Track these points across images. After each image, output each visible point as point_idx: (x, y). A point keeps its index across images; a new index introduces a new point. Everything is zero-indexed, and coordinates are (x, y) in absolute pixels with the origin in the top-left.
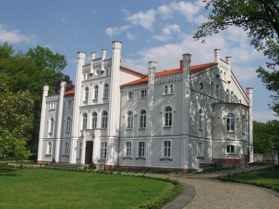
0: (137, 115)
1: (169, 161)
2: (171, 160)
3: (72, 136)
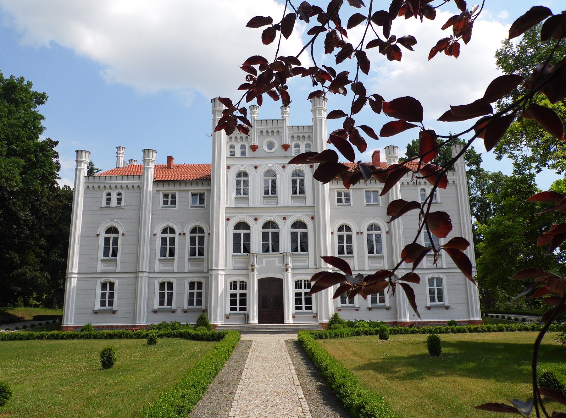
2: (447, 308)
3: (214, 268)
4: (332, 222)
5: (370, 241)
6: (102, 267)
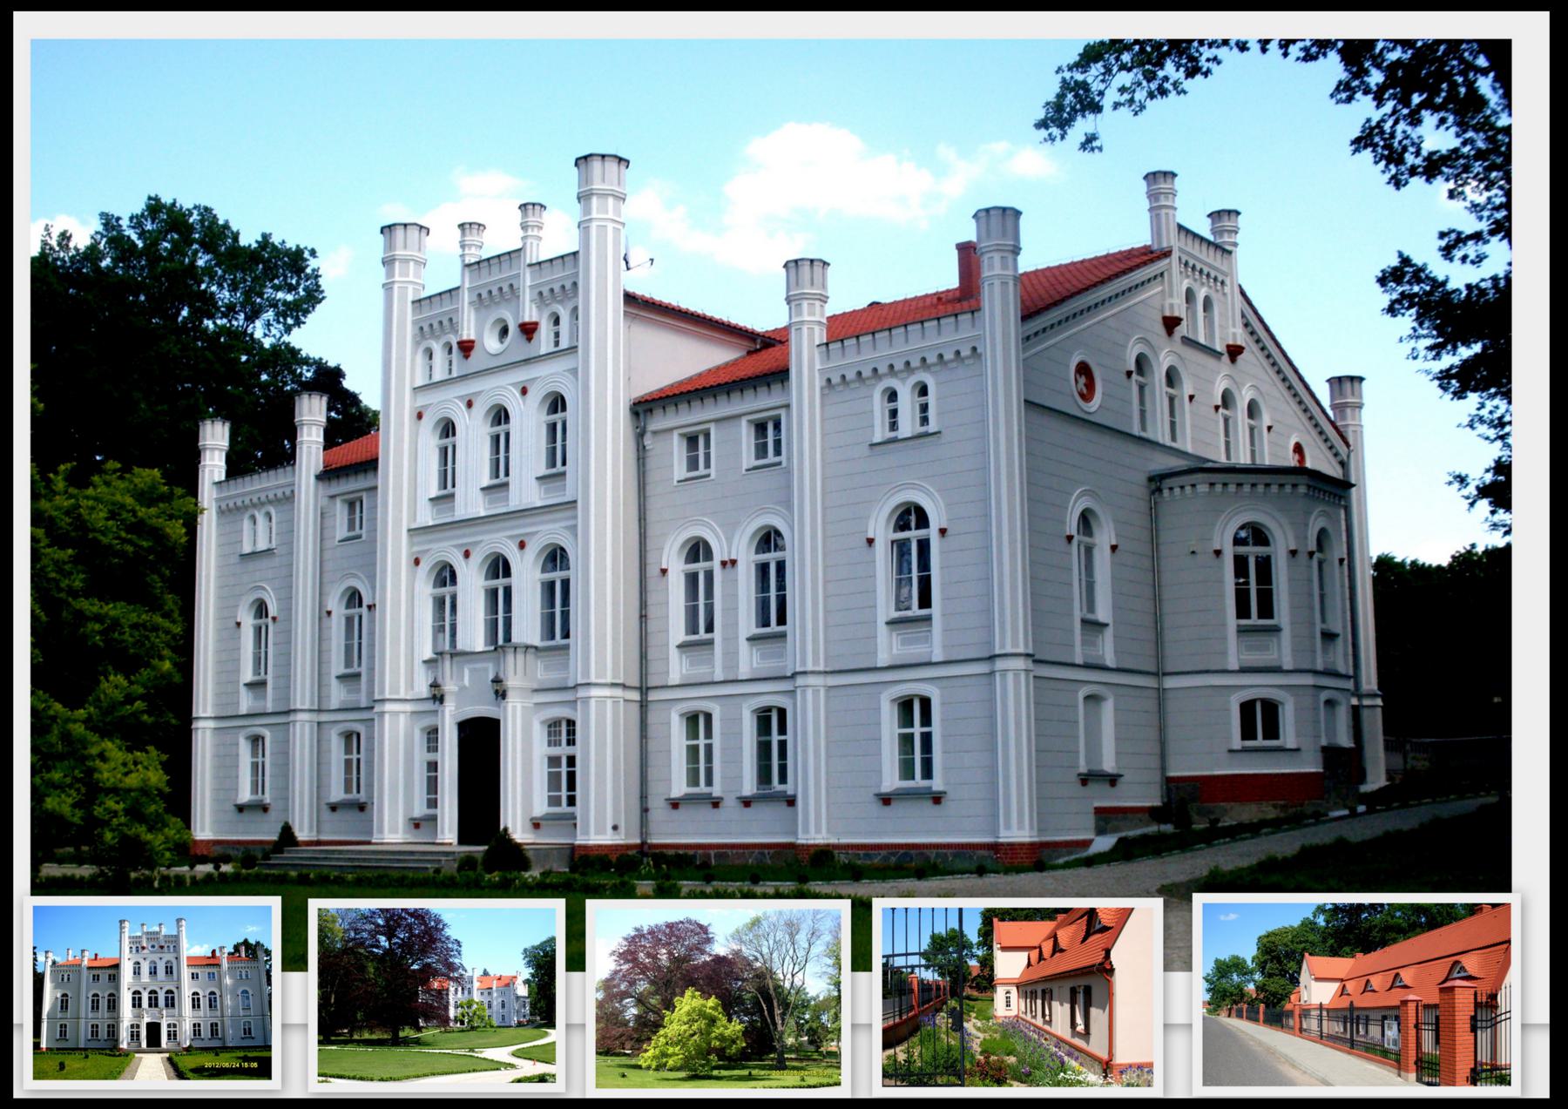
0: (734, 562)
2: (937, 799)
4: (189, 989)
5: (210, 1000)
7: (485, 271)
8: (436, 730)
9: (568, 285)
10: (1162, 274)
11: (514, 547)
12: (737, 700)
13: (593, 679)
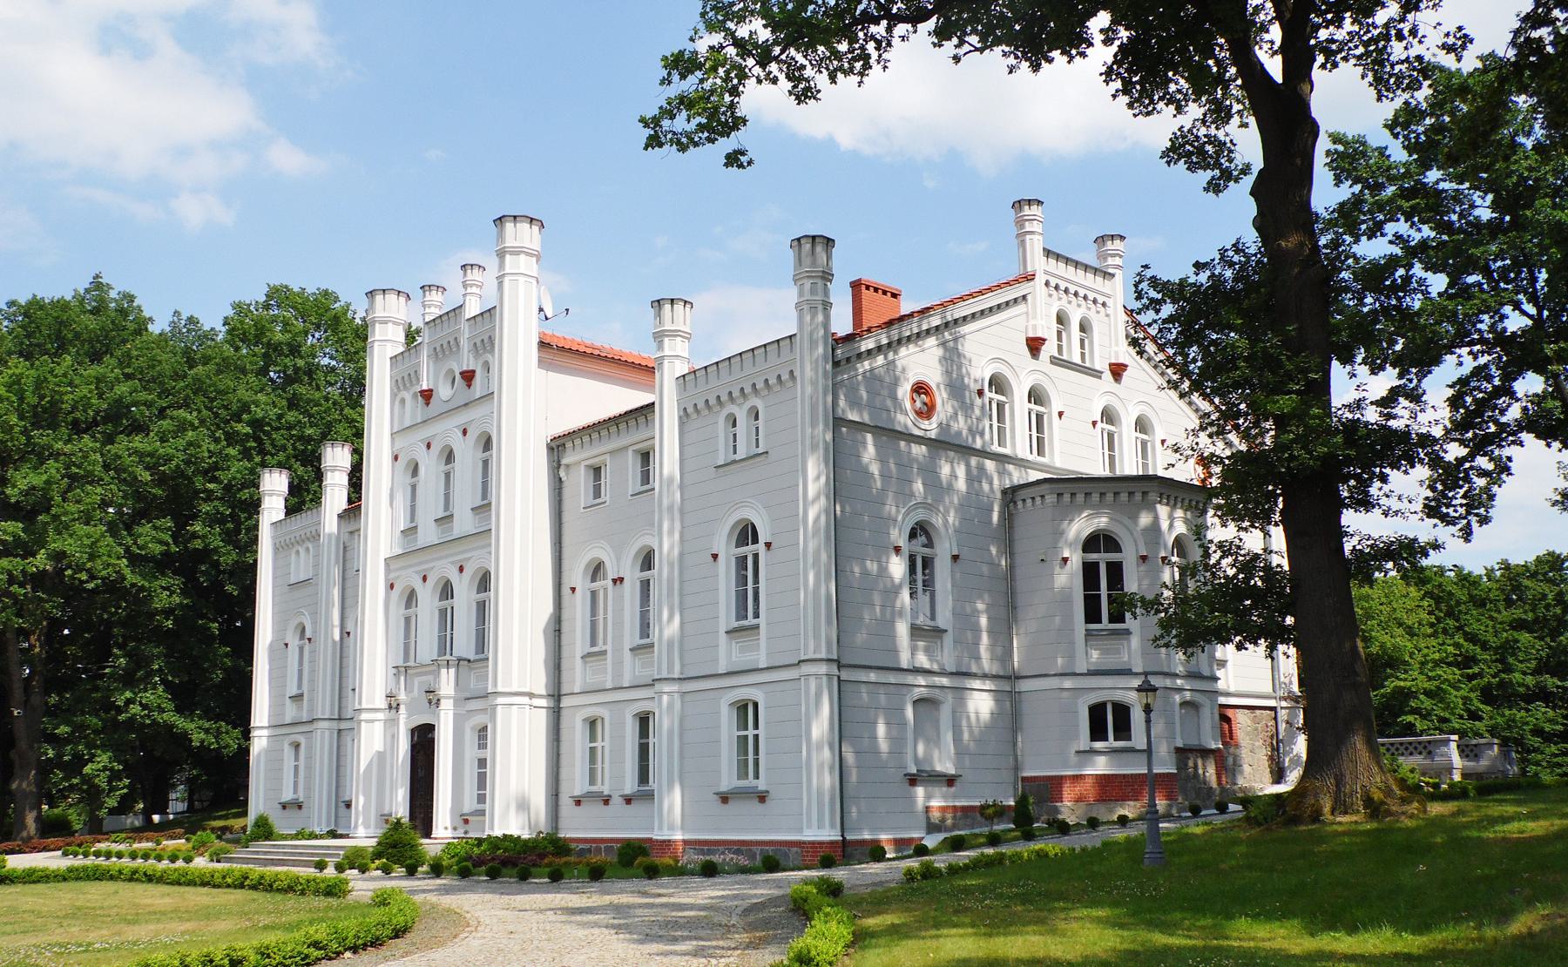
0: (621, 579)
1: (755, 806)
2: (762, 798)
6: (734, 655)
7: (439, 328)
8: (485, 729)
9: (486, 338)
10: (1024, 297)
11: (455, 570)
12: (622, 704)
13: (500, 689)
